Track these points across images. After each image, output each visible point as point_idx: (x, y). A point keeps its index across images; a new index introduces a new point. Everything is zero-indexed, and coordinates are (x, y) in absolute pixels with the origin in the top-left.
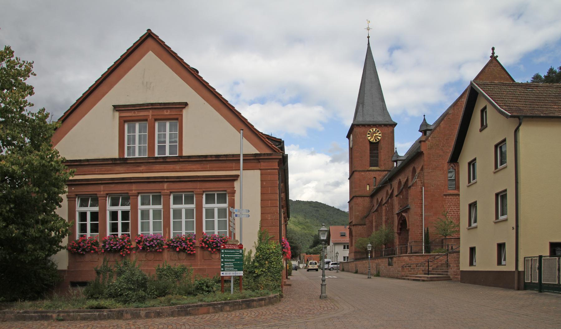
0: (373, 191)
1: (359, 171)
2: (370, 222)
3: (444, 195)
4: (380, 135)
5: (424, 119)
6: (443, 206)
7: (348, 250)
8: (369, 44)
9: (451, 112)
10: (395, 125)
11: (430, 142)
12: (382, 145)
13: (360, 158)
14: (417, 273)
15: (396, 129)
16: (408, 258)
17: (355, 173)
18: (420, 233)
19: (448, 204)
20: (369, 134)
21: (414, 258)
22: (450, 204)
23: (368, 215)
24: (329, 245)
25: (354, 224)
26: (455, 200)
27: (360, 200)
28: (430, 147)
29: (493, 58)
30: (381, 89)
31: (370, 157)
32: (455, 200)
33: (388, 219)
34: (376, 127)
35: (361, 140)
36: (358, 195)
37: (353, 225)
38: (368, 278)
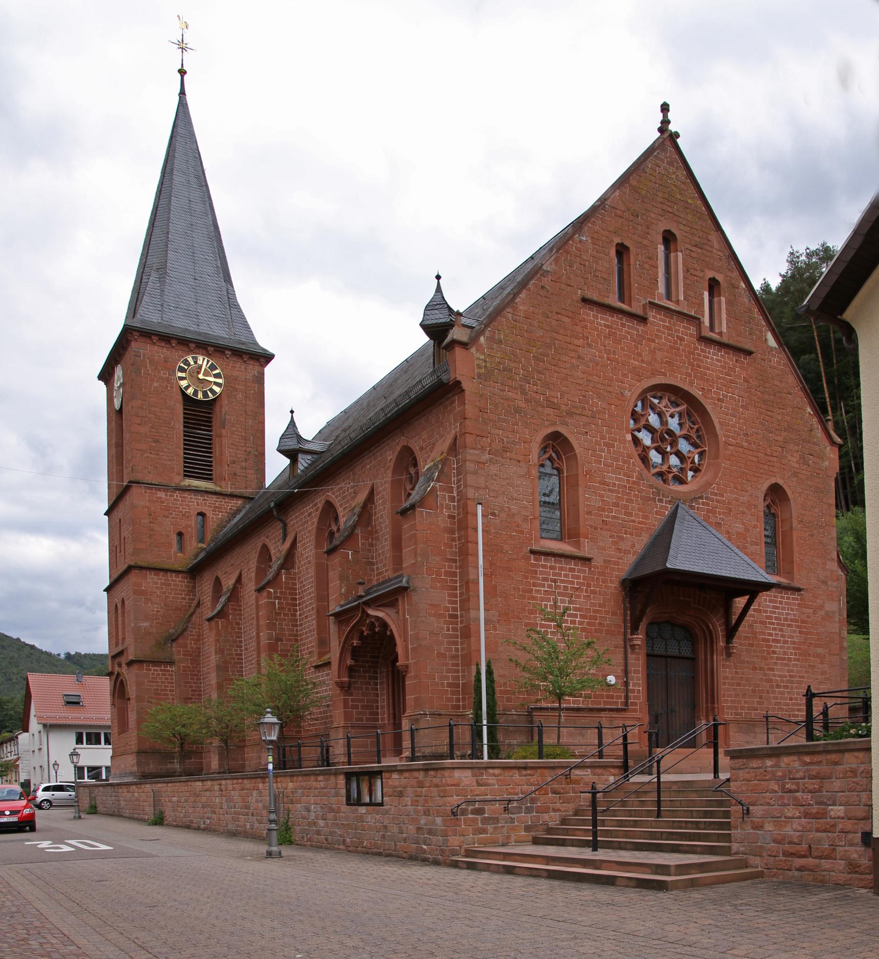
0: (197, 555)
1: (150, 485)
2: (189, 655)
3: (532, 552)
4: (220, 381)
5: (439, 290)
6: (531, 591)
7: (110, 746)
8: (182, 93)
9: (549, 269)
10: (268, 358)
11: (484, 354)
12: (226, 412)
13: (154, 445)
14: (508, 837)
15: (269, 370)
16: (474, 775)
17: (135, 490)
18: (449, 685)
19: (543, 586)
20: (182, 370)
21: (494, 775)
22: (550, 586)
23: (184, 630)
24: (26, 729)
25: (131, 657)
26: (565, 576)
27: (152, 581)
28: (483, 371)
29: (666, 135)
30: (222, 243)
31: (185, 449)
32: (565, 576)
33: (278, 639)
34: (208, 351)
35: (156, 384)
36: (143, 564)
37: (130, 664)
38: (270, 854)
